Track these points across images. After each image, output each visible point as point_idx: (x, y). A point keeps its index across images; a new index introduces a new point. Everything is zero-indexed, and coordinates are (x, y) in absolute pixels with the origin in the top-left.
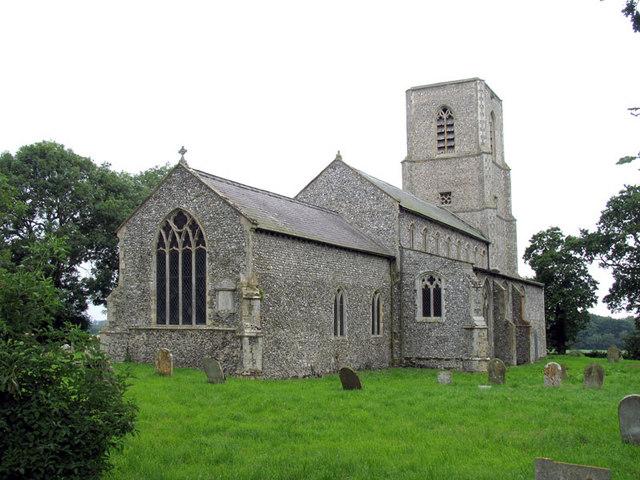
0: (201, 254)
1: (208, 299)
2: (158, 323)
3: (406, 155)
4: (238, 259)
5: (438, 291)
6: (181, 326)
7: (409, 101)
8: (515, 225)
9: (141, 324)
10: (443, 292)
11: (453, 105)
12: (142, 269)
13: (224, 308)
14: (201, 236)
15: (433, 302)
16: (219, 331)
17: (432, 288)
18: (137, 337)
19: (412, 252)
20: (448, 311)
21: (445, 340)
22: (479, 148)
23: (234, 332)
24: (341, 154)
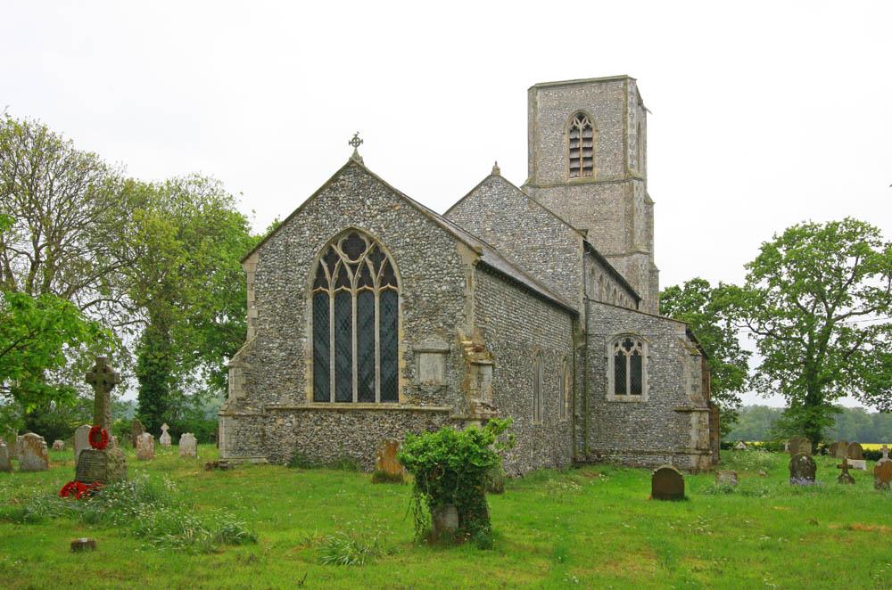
0: (389, 298)
1: (402, 364)
2: (315, 400)
3: (527, 177)
4: (452, 306)
5: (637, 359)
6: (356, 404)
7: (532, 103)
8: (657, 277)
9: (287, 401)
10: (645, 361)
11: (592, 109)
12: (289, 318)
13: (431, 377)
14: (389, 269)
15: (629, 374)
16: (422, 412)
17: (628, 355)
18: (280, 421)
19: (601, 306)
20: (652, 388)
21: (649, 426)
22: (626, 171)
23: (446, 413)
24: (499, 165)
